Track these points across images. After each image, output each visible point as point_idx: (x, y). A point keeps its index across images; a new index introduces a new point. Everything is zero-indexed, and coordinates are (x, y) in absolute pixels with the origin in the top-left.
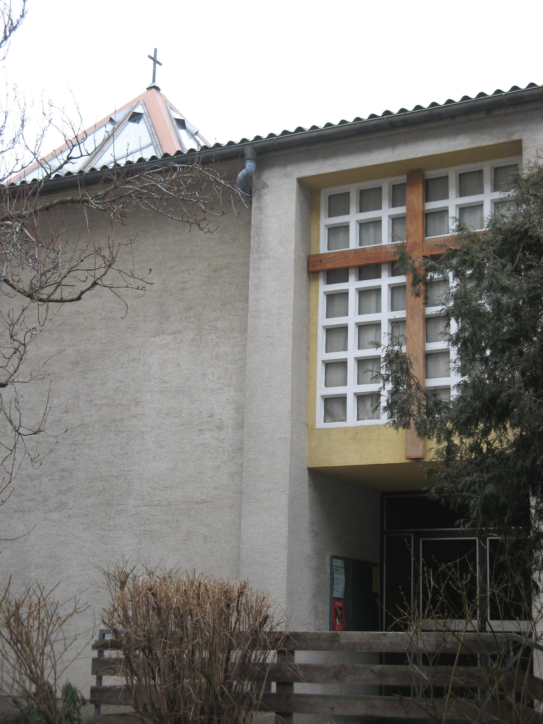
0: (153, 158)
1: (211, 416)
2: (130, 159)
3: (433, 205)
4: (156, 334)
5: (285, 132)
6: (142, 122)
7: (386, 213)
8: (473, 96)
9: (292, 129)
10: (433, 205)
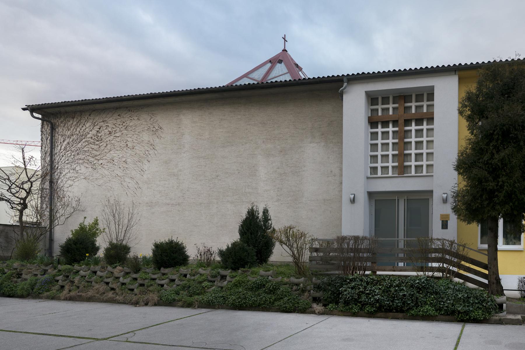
0: (290, 80)
1: (331, 172)
2: (272, 80)
3: (407, 128)
4: (311, 143)
5: (323, 77)
6: (283, 63)
7: (391, 106)
8: (469, 64)
9: (197, 88)
10: (407, 128)
